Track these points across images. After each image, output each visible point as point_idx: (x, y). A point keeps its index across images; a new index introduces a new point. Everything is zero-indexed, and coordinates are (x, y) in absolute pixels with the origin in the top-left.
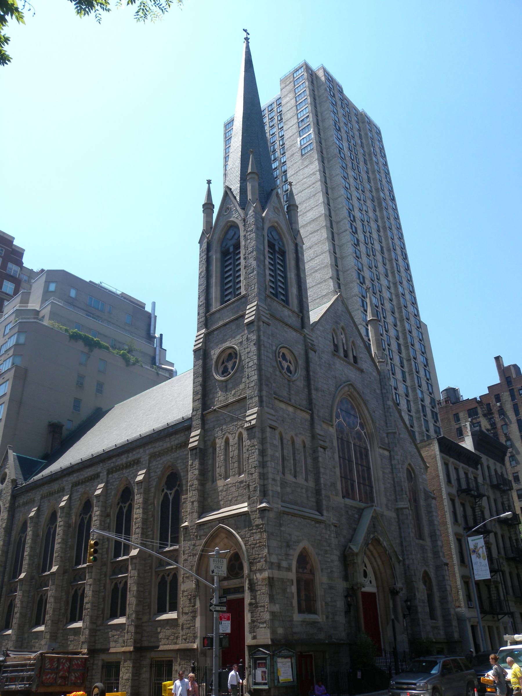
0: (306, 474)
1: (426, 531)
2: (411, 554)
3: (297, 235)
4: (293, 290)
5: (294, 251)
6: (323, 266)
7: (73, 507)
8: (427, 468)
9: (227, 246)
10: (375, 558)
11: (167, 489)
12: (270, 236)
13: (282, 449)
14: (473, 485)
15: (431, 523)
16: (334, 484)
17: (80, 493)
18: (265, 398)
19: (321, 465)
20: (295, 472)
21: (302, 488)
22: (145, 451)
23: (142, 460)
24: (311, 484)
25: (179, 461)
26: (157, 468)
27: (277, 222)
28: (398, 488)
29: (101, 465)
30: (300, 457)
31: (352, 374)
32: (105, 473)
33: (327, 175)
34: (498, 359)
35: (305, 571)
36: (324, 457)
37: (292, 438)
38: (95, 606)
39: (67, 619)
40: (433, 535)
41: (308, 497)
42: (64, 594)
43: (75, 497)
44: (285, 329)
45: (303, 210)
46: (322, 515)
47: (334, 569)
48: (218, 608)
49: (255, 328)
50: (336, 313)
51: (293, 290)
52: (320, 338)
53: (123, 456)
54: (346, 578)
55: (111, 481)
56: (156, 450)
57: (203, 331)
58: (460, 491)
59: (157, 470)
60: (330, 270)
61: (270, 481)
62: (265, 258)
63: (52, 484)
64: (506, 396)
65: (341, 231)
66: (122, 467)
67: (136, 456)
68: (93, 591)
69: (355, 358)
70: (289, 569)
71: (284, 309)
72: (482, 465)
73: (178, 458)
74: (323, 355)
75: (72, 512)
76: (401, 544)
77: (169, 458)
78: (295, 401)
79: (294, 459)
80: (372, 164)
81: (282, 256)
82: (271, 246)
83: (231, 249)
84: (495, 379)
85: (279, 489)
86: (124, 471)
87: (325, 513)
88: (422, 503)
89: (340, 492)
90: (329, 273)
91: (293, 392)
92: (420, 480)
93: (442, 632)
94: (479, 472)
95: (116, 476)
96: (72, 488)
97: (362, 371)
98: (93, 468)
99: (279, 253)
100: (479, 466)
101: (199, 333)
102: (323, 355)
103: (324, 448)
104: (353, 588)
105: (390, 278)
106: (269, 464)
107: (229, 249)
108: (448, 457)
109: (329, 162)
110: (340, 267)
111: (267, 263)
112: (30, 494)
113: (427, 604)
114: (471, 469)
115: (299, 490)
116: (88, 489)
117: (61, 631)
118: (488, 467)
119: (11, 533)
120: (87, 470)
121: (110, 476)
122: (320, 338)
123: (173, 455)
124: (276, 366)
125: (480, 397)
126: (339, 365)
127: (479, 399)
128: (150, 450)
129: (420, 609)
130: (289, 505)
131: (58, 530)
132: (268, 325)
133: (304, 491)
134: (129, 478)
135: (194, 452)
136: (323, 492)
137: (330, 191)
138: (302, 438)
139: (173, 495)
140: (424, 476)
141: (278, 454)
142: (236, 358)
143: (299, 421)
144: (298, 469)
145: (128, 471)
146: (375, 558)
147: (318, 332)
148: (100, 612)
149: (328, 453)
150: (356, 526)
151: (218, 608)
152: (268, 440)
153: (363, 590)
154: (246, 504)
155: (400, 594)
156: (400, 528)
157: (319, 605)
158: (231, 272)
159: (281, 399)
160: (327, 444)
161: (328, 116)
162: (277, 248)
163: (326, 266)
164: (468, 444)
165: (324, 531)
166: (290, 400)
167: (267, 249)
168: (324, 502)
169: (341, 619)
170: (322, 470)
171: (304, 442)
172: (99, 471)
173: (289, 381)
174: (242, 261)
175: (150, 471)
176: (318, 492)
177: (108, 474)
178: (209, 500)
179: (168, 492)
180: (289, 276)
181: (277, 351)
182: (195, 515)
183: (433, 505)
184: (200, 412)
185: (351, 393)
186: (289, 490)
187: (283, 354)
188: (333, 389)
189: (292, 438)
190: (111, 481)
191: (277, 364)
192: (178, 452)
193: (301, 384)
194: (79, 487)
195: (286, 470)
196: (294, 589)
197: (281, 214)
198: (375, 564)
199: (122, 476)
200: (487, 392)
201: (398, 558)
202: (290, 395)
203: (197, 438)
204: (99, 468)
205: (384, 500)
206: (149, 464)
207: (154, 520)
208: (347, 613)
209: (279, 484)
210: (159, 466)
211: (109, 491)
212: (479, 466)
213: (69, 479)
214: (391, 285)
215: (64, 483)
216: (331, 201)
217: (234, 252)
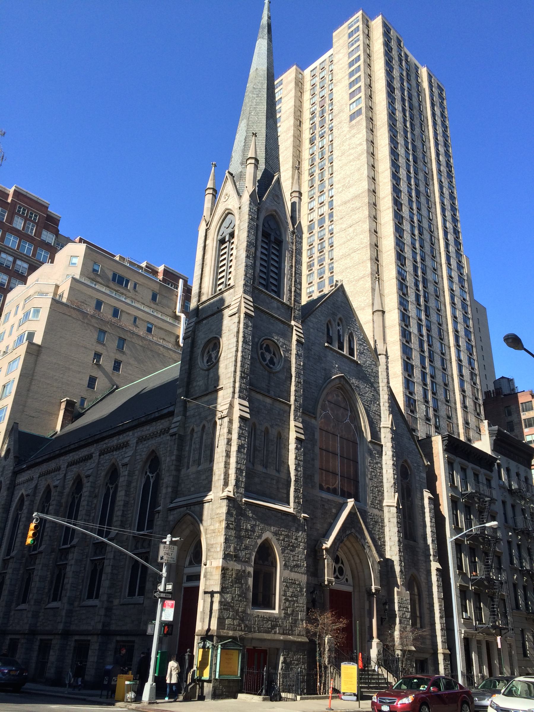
7: (66, 486)
10: (352, 556)
11: (150, 473)
12: (266, 225)
17: (73, 473)
22: (133, 434)
23: (130, 442)
25: (162, 446)
26: (143, 451)
27: (275, 211)
29: (95, 445)
32: (98, 454)
37: (267, 429)
38: (74, 587)
39: (49, 598)
41: (278, 488)
42: (49, 573)
43: (69, 477)
44: (272, 321)
45: (346, 184)
50: (334, 304)
52: (312, 330)
53: (115, 438)
55: (102, 462)
56: (143, 433)
57: (194, 319)
59: (143, 453)
60: (369, 251)
63: (50, 462)
66: (112, 448)
67: (126, 439)
68: (73, 572)
71: (273, 300)
73: (161, 442)
74: (313, 347)
75: (65, 491)
77: (154, 442)
78: (274, 392)
82: (266, 235)
83: (227, 239)
86: (115, 453)
90: (368, 254)
91: (273, 384)
92: (418, 478)
95: (107, 457)
96: (67, 467)
98: (87, 448)
99: (275, 243)
101: (190, 321)
102: (313, 347)
107: (225, 238)
108: (453, 457)
114: (483, 471)
116: (81, 469)
117: (43, 611)
119: (9, 510)
120: (82, 450)
121: (102, 457)
122: (312, 330)
123: (157, 439)
124: (257, 358)
128: (138, 433)
133: (275, 482)
134: (118, 460)
143: (277, 412)
145: (118, 453)
146: (352, 556)
147: (310, 324)
148: (78, 593)
150: (332, 521)
159: (258, 390)
162: (272, 238)
163: (366, 247)
166: (269, 391)
172: (92, 451)
173: (270, 373)
175: (137, 454)
177: (100, 455)
178: (183, 486)
179: (150, 475)
181: (259, 343)
182: (168, 500)
185: (343, 386)
187: (267, 345)
188: (321, 382)
189: (267, 429)
190: (102, 462)
191: (258, 357)
192: (162, 436)
194: (73, 467)
196: (250, 581)
198: (353, 561)
199: (111, 458)
202: (269, 386)
203: (178, 424)
204: (92, 449)
206: (136, 447)
207: (134, 503)
210: (145, 450)
211: (99, 473)
213: (66, 458)
215: (61, 462)
217: (229, 241)
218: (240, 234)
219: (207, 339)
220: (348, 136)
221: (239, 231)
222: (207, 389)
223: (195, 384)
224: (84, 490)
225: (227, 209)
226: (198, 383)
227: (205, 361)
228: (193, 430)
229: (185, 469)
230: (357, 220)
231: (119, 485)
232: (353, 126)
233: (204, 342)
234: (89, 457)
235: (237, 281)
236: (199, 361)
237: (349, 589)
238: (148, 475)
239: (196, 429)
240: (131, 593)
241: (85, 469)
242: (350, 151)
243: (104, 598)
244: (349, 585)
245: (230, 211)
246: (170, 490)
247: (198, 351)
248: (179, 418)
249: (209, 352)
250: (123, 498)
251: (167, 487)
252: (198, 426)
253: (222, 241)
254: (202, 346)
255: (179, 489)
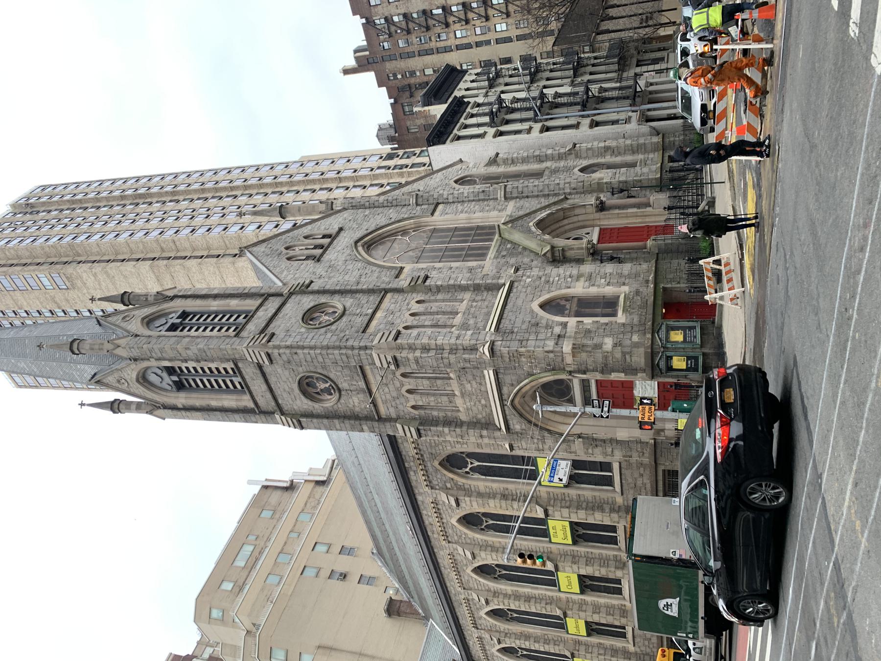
0: (456, 300)
1: (535, 167)
2: (558, 184)
3: (162, 294)
4: (234, 304)
5: (183, 300)
6: (217, 273)
8: (461, 161)
9: (171, 383)
11: (466, 467)
13: (424, 326)
14: (486, 109)
15: (525, 160)
16: (471, 270)
18: (362, 344)
19: (446, 283)
20: (451, 313)
21: (472, 306)
24: (467, 296)
27: (143, 319)
28: (481, 196)
30: (435, 307)
31: (345, 241)
33: (98, 258)
34: (346, 72)
35: (568, 307)
36: (437, 279)
37: (412, 315)
40: (540, 159)
46: (504, 284)
47: (568, 273)
48: (606, 409)
49: (276, 351)
51: (234, 304)
54: (579, 261)
55: (456, 538)
57: (277, 416)
58: (492, 124)
61: (458, 342)
62: (188, 336)
64: (390, 66)
65: (174, 247)
69: (324, 237)
70: (565, 325)
72: (463, 97)
76: (547, 196)
79: (437, 313)
80: (88, 201)
81: (188, 316)
83: (175, 378)
84: (370, 77)
85: (469, 333)
87: (501, 281)
88: (501, 169)
89: (480, 263)
93: (651, 156)
94: (472, 100)
97: (341, 229)
99: (184, 320)
100: (466, 100)
103: (427, 277)
104: (593, 254)
105: (238, 193)
106: (439, 342)
107: (174, 382)
109: (79, 255)
110: (221, 252)
111: (196, 334)
112: (471, 643)
113: (618, 170)
114: (468, 110)
115: (473, 310)
118: (467, 89)
125: (390, 98)
126: (331, 255)
127: (392, 101)
129: (623, 178)
130: (490, 322)
131: (513, 607)
132: (273, 335)
133: (474, 304)
135: (422, 432)
136: (477, 282)
137: (121, 257)
138: (412, 303)
139: (474, 461)
140: (471, 166)
141: (429, 331)
142: (312, 377)
144: (449, 310)
147: (289, 278)
149: (433, 274)
151: (606, 409)
152: (411, 341)
153: (595, 242)
154: (486, 372)
155: (603, 199)
156: (527, 197)
157: (609, 291)
158: (205, 380)
160: (422, 275)
161: (12, 251)
164: (438, 110)
165: (522, 283)
167: (177, 333)
168: (489, 281)
169: (627, 268)
170: (452, 282)
171: (418, 302)
174: (191, 365)
176: (477, 288)
178: (480, 416)
179: (470, 466)
180: (215, 308)
182: (497, 434)
183: (505, 157)
184: (376, 424)
186: (471, 322)
193: (349, 301)
195: (449, 323)
196: (588, 320)
197: (133, 313)
200: (384, 89)
201: (562, 200)
203: (406, 428)
205: (495, 213)
208: (620, 261)
209: (464, 332)
211: (469, 541)
212: (466, 100)
214: (247, 192)
216: (134, 256)
217: (178, 376)
218: (167, 357)
219: (302, 397)
220: (85, 291)
221: (165, 359)
222: (362, 390)
223: (357, 409)
224: (513, 645)
225: (138, 381)
226: (356, 404)
227: (329, 397)
228: (413, 407)
229: (459, 414)
230: (187, 278)
231: (496, 563)
232: (72, 285)
233: (305, 401)
234: (480, 638)
235: (227, 357)
236: (328, 405)
237: (597, 230)
238: (471, 469)
239: (413, 403)
240: (609, 481)
241: (465, 562)
242: (103, 288)
243: (615, 516)
244: (593, 231)
245: (141, 375)
246: (485, 433)
247: (317, 407)
248: (399, 426)
249: (318, 393)
250: (497, 501)
251: (481, 436)
252: (407, 400)
253: (180, 386)
254: (310, 403)
255: (483, 421)
